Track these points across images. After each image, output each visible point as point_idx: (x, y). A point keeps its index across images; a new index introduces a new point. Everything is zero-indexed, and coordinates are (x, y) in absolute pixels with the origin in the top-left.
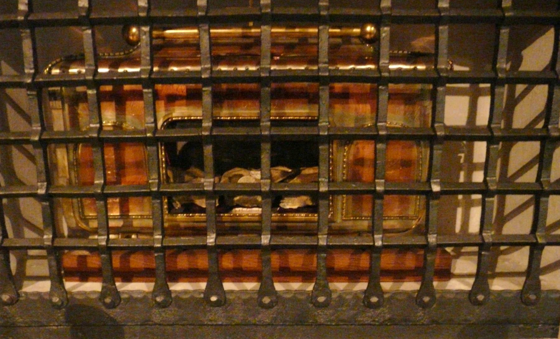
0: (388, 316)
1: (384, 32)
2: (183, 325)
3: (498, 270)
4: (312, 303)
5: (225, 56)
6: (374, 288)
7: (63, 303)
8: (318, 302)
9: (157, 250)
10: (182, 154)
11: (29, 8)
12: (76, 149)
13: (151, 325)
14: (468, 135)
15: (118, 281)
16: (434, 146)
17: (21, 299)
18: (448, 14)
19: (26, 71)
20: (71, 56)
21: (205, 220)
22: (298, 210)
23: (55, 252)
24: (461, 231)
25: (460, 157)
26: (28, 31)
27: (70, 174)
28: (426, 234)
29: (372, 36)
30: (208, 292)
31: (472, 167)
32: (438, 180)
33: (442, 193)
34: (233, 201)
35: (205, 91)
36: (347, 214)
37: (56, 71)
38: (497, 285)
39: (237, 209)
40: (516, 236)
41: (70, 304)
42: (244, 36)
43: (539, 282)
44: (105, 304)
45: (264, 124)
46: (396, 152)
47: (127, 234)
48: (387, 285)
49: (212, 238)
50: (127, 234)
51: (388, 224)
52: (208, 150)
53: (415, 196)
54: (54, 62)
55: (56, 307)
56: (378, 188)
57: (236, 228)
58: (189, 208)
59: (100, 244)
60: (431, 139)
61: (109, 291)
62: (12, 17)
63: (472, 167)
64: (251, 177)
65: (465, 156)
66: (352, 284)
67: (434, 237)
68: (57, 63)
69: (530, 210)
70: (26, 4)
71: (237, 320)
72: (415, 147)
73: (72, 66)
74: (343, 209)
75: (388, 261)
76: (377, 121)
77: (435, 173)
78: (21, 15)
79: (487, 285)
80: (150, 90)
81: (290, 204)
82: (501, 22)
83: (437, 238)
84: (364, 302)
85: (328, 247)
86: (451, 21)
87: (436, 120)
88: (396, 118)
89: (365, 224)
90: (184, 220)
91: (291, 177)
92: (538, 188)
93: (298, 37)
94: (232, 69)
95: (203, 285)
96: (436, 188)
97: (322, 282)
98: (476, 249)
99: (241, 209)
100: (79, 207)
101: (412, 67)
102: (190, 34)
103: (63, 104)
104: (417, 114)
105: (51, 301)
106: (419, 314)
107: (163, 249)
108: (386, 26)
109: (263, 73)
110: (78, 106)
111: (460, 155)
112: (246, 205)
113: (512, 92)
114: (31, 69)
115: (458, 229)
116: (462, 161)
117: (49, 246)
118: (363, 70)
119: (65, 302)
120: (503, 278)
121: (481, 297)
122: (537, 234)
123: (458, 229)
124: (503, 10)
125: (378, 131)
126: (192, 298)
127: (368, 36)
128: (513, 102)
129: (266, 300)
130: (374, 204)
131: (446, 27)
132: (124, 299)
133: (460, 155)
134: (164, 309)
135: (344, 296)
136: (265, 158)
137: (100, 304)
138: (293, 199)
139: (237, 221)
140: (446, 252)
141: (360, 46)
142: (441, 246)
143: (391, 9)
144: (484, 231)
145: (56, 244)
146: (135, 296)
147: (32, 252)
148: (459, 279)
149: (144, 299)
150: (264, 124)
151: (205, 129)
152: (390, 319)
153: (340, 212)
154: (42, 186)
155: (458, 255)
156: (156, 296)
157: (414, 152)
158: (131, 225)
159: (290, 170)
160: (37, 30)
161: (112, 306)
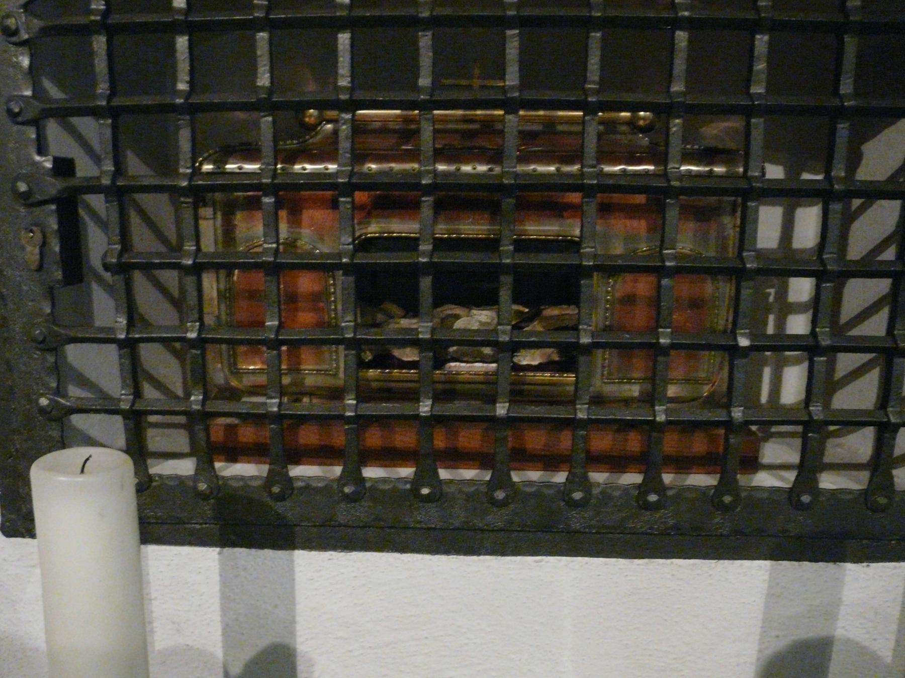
0: (671, 522)
1: (675, 126)
2: (382, 528)
3: (827, 459)
4: (564, 501)
5: (443, 149)
6: (652, 483)
7: (211, 493)
8: (572, 499)
9: (349, 420)
10: (381, 283)
11: (190, 86)
12: (230, 275)
13: (334, 527)
14: (785, 264)
15: (220, 461)
16: (743, 283)
17: (154, 484)
18: (763, 102)
19: (181, 170)
20: (229, 146)
21: (417, 379)
22: (540, 368)
23: (196, 421)
24: (768, 402)
25: (769, 294)
26: (188, 117)
27: (219, 309)
28: (728, 406)
29: (648, 122)
30: (417, 482)
31: (786, 309)
32: (747, 331)
33: (751, 348)
34: (447, 353)
35: (425, 201)
36: (610, 373)
37: (208, 167)
38: (828, 482)
39: (452, 364)
40: (855, 412)
41: (220, 495)
42: (466, 120)
43: (891, 477)
44: (271, 494)
45: (506, 248)
46: (684, 288)
47: (295, 397)
48: (599, 477)
49: (426, 406)
50: (295, 397)
51: (672, 391)
52: (426, 283)
53: (707, 353)
54: (206, 155)
55: (204, 496)
56: (662, 341)
57: (449, 391)
58: (384, 360)
59: (270, 409)
60: (737, 273)
61: (278, 476)
62: (167, 100)
63: (786, 309)
64: (478, 319)
65: (776, 293)
66: (615, 475)
67: (739, 411)
68: (210, 155)
69: (874, 375)
70: (187, 82)
71: (457, 523)
72: (709, 281)
73: (231, 160)
74: (603, 367)
75: (670, 443)
76: (662, 247)
77: (742, 321)
78: (180, 98)
79: (816, 481)
80: (349, 199)
81: (528, 358)
82: (839, 113)
83: (743, 412)
84: (637, 502)
85: (590, 421)
86: (767, 111)
87: (746, 247)
88: (685, 241)
89: (635, 390)
90: (377, 377)
91: (530, 319)
92: (889, 344)
93: (543, 124)
94: (452, 168)
95: (338, 470)
96: (744, 342)
97: (578, 471)
98: (800, 428)
99: (458, 364)
100: (230, 356)
101: (707, 169)
102: (388, 116)
103: (215, 213)
104: (713, 234)
105: (195, 488)
106: (717, 520)
107: (358, 417)
108: (678, 117)
109: (507, 179)
110: (233, 214)
111: (768, 290)
112: (465, 359)
113: (847, 207)
114: (188, 168)
115: (764, 398)
116: (771, 299)
117: (199, 410)
118: (636, 174)
119: (215, 493)
120: (837, 472)
121: (806, 499)
122: (890, 409)
123: (764, 398)
124: (841, 98)
125: (663, 261)
126: (394, 490)
127: (641, 123)
128: (849, 218)
129: (500, 495)
130: (655, 362)
131: (762, 120)
132: (301, 488)
133: (768, 290)
134: (353, 505)
135: (609, 491)
136: (505, 295)
137: (265, 494)
138: (533, 351)
139: (452, 380)
140: (750, 430)
141: (630, 137)
142: (747, 423)
143: (684, 94)
144: (811, 404)
145: (208, 409)
146: (314, 484)
147: (153, 419)
148: (771, 472)
149: (328, 489)
150: (506, 248)
151: (424, 254)
152: (674, 527)
153: (599, 371)
154: (193, 327)
155: (768, 436)
156: (345, 485)
157: (709, 287)
158: (302, 383)
159: (527, 310)
160: (199, 116)
161: (281, 498)
